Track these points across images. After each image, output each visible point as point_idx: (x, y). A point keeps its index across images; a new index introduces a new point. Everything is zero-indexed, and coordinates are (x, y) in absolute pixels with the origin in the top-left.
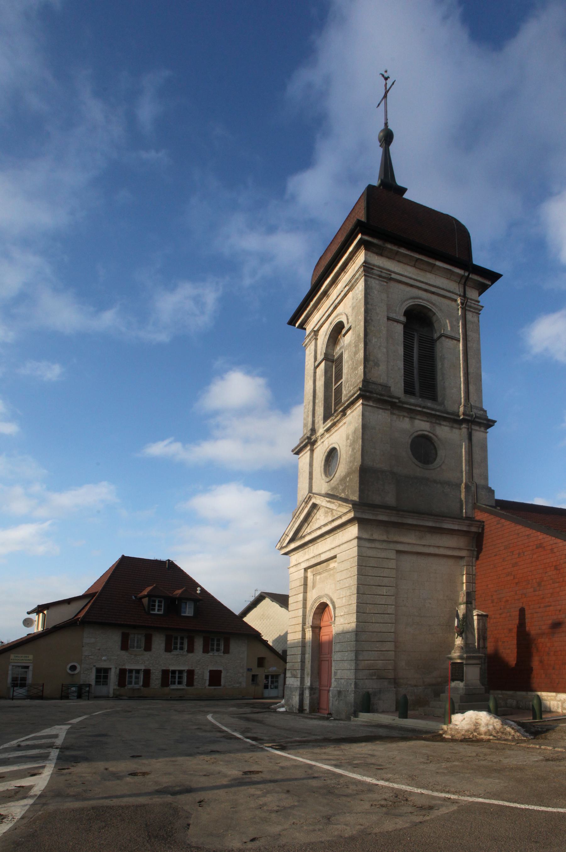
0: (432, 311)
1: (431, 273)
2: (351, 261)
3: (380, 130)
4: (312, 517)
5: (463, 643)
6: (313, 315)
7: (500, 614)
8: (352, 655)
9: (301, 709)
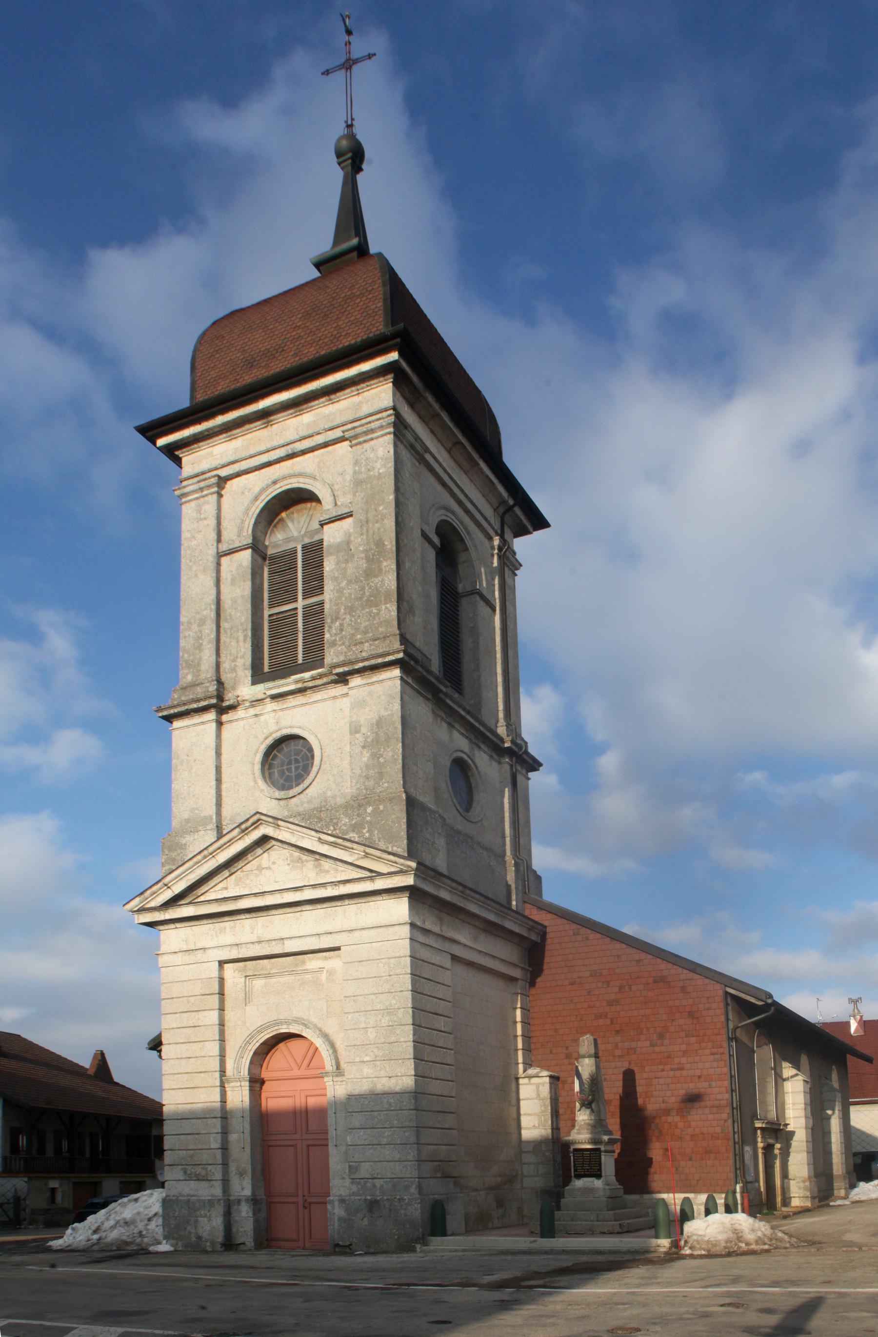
0: (465, 543)
1: (466, 474)
2: (354, 388)
4: (246, 862)
5: (593, 1118)
8: (410, 1136)
9: (229, 1244)
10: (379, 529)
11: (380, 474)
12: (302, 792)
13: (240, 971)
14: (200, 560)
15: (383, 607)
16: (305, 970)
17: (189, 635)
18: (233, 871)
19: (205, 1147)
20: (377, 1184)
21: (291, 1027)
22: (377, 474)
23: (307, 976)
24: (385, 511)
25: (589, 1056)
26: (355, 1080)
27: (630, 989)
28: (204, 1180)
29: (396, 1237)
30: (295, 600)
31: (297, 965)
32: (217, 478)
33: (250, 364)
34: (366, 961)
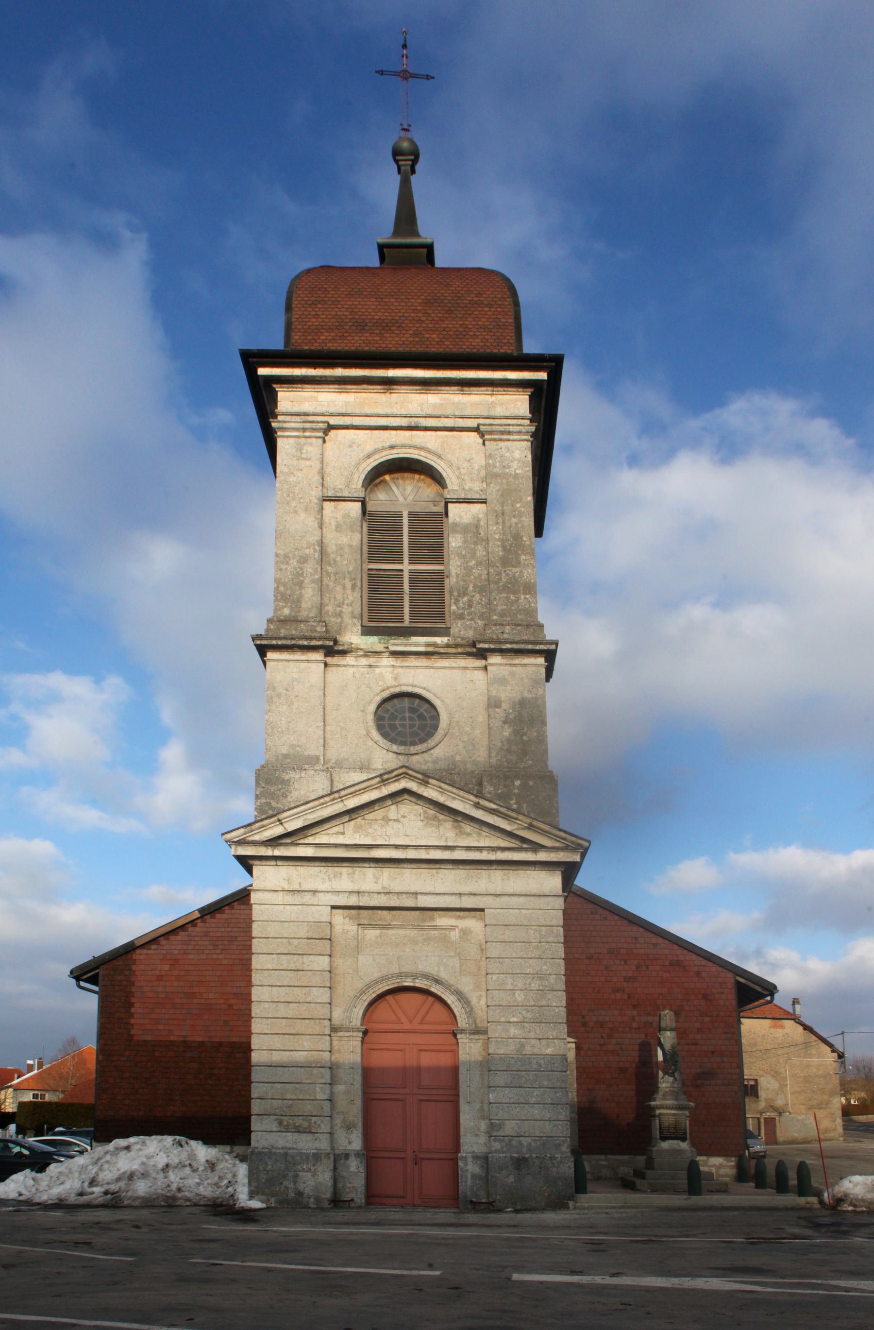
2: (490, 389)
3: (420, 149)
6: (320, 386)
7: (601, 1045)
9: (337, 1202)
10: (516, 524)
11: (516, 474)
12: (425, 752)
13: (351, 918)
14: (301, 498)
15: (523, 597)
16: (433, 926)
17: (286, 569)
18: (354, 817)
19: (308, 1097)
20: (523, 1142)
21: (417, 981)
22: (513, 473)
23: (433, 932)
24: (522, 509)
25: (671, 1030)
26: (499, 1040)
27: (647, 968)
28: (306, 1132)
29: (546, 1194)
30: (411, 563)
31: (424, 920)
32: (326, 425)
33: (361, 326)
34: (514, 925)
